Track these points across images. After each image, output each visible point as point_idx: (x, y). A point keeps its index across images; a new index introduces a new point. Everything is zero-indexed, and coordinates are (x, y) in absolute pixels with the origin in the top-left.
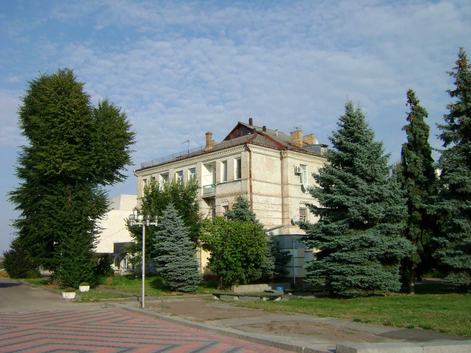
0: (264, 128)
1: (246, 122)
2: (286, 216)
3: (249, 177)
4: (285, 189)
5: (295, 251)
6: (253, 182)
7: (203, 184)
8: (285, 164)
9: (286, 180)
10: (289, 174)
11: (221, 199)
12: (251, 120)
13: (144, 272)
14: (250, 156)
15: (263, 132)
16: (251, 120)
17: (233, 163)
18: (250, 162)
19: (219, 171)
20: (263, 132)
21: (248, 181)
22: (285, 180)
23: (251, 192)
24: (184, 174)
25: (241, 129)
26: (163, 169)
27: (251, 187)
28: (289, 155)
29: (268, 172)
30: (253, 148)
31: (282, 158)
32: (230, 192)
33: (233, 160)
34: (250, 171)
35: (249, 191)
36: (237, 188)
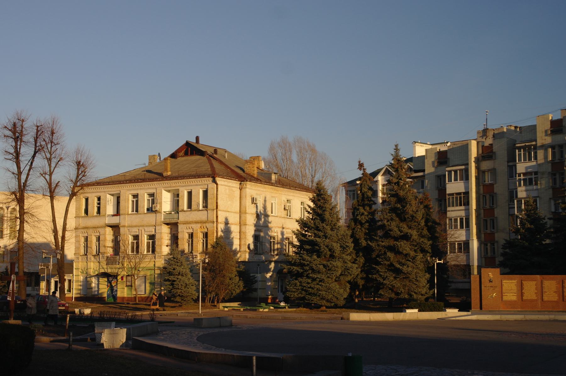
0: (215, 151)
1: (193, 140)
2: (243, 242)
3: (215, 208)
4: (243, 218)
5: (259, 275)
6: (219, 213)
7: (163, 210)
8: (243, 194)
9: (244, 209)
10: (247, 204)
11: (185, 225)
12: (197, 138)
13: (552, 317)
14: (217, 188)
15: (215, 155)
16: (197, 138)
17: (199, 193)
18: (217, 194)
19: (183, 199)
20: (215, 155)
21: (215, 211)
22: (243, 209)
23: (217, 221)
24: (139, 197)
25: (190, 149)
26: (115, 189)
27: (217, 217)
28: (248, 186)
29: (229, 203)
30: (218, 180)
31: (241, 189)
32: (195, 220)
33: (199, 190)
34: (217, 203)
35: (215, 220)
36: (202, 215)
